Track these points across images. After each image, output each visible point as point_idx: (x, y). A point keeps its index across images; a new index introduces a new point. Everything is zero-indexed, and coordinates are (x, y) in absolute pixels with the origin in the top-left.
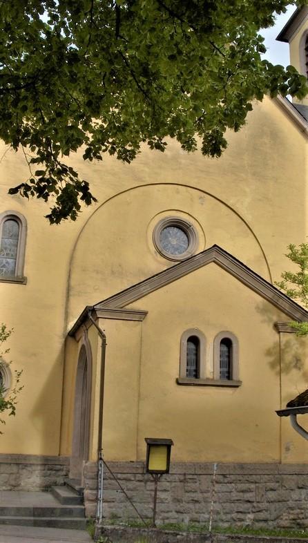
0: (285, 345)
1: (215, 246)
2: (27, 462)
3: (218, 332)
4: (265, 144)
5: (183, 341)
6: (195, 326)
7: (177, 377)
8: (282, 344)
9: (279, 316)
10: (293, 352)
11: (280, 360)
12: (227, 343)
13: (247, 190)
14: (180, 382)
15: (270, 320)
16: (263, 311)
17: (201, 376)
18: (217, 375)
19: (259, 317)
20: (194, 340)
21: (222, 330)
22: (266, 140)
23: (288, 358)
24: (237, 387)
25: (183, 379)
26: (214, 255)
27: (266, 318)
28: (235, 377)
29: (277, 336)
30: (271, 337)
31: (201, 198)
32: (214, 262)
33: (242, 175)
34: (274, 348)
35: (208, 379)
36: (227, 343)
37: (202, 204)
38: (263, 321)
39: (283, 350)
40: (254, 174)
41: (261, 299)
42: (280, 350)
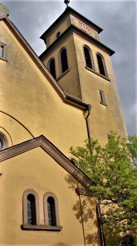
0: (83, 203)
1: (42, 135)
2: (79, 201)
3: (45, 193)
4: (44, 98)
5: (24, 198)
6: (32, 188)
7: (22, 224)
8: (82, 202)
9: (77, 184)
10: (88, 208)
11: (81, 213)
12: (51, 201)
13: (35, 120)
14: (25, 227)
15: (73, 187)
16: (69, 181)
17: (38, 223)
18: (47, 223)
19: (67, 185)
20: (31, 198)
21: (47, 191)
22: (44, 97)
23: (86, 212)
24: (59, 231)
25: (26, 225)
26: (41, 141)
27: (70, 185)
28: (58, 224)
29: (78, 197)
30: (75, 198)
31: (10, 120)
32: (40, 146)
33: (33, 112)
34: (77, 205)
35: (41, 225)
36: (51, 201)
37: (11, 124)
38: (70, 188)
39: (83, 206)
40: (38, 113)
41: (67, 173)
42: (81, 206)
